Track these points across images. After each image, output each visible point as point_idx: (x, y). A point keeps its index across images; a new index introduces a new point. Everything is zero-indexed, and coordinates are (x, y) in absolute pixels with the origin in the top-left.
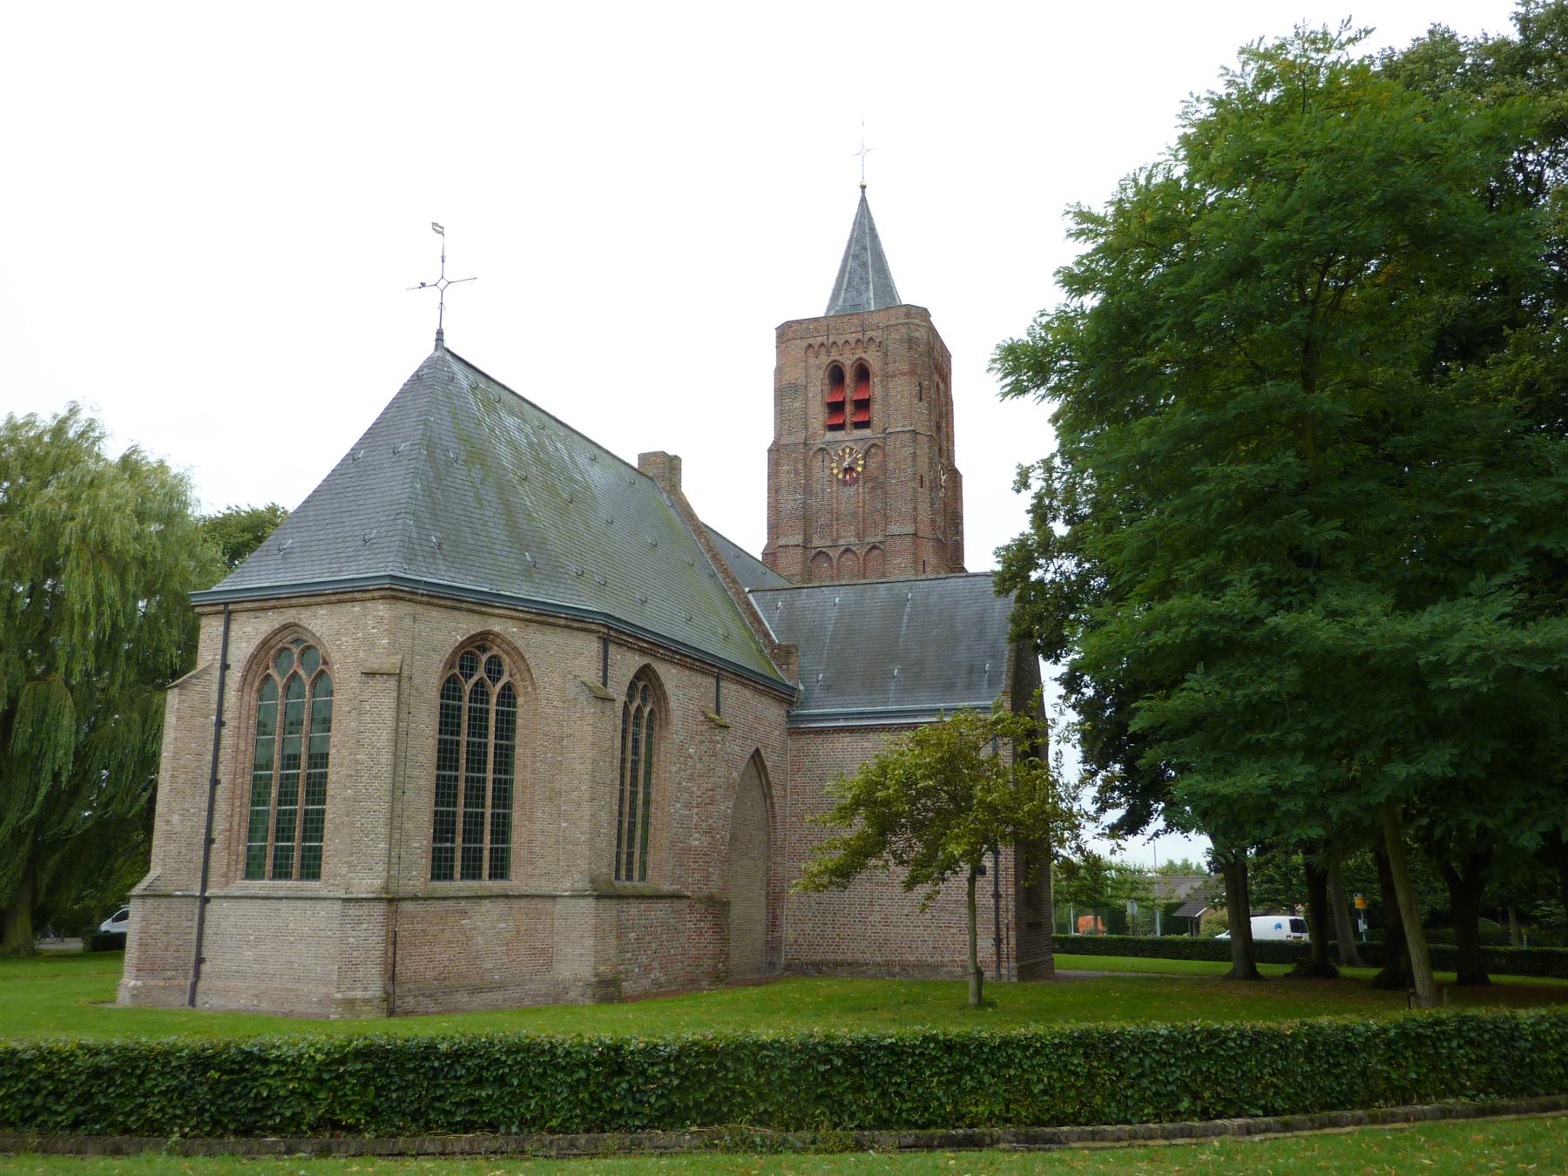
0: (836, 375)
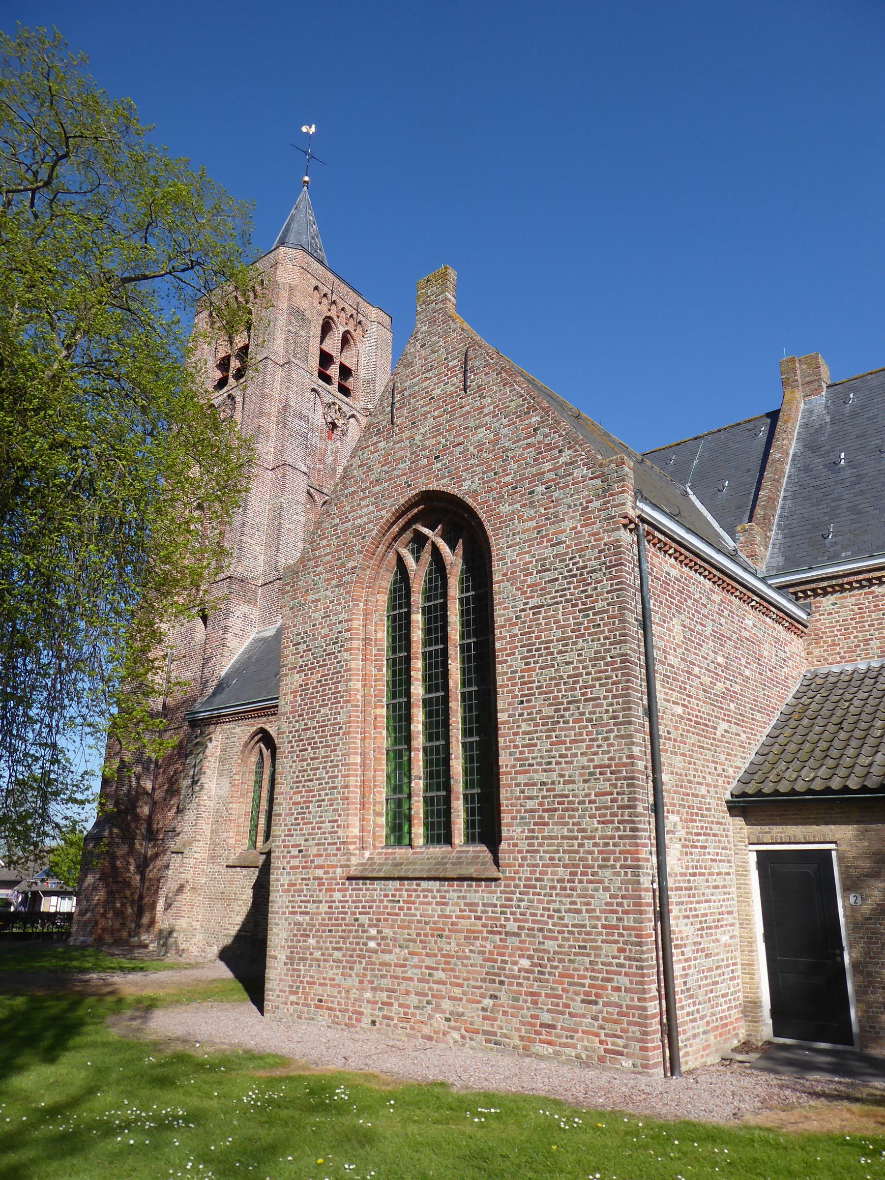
0: (327, 327)
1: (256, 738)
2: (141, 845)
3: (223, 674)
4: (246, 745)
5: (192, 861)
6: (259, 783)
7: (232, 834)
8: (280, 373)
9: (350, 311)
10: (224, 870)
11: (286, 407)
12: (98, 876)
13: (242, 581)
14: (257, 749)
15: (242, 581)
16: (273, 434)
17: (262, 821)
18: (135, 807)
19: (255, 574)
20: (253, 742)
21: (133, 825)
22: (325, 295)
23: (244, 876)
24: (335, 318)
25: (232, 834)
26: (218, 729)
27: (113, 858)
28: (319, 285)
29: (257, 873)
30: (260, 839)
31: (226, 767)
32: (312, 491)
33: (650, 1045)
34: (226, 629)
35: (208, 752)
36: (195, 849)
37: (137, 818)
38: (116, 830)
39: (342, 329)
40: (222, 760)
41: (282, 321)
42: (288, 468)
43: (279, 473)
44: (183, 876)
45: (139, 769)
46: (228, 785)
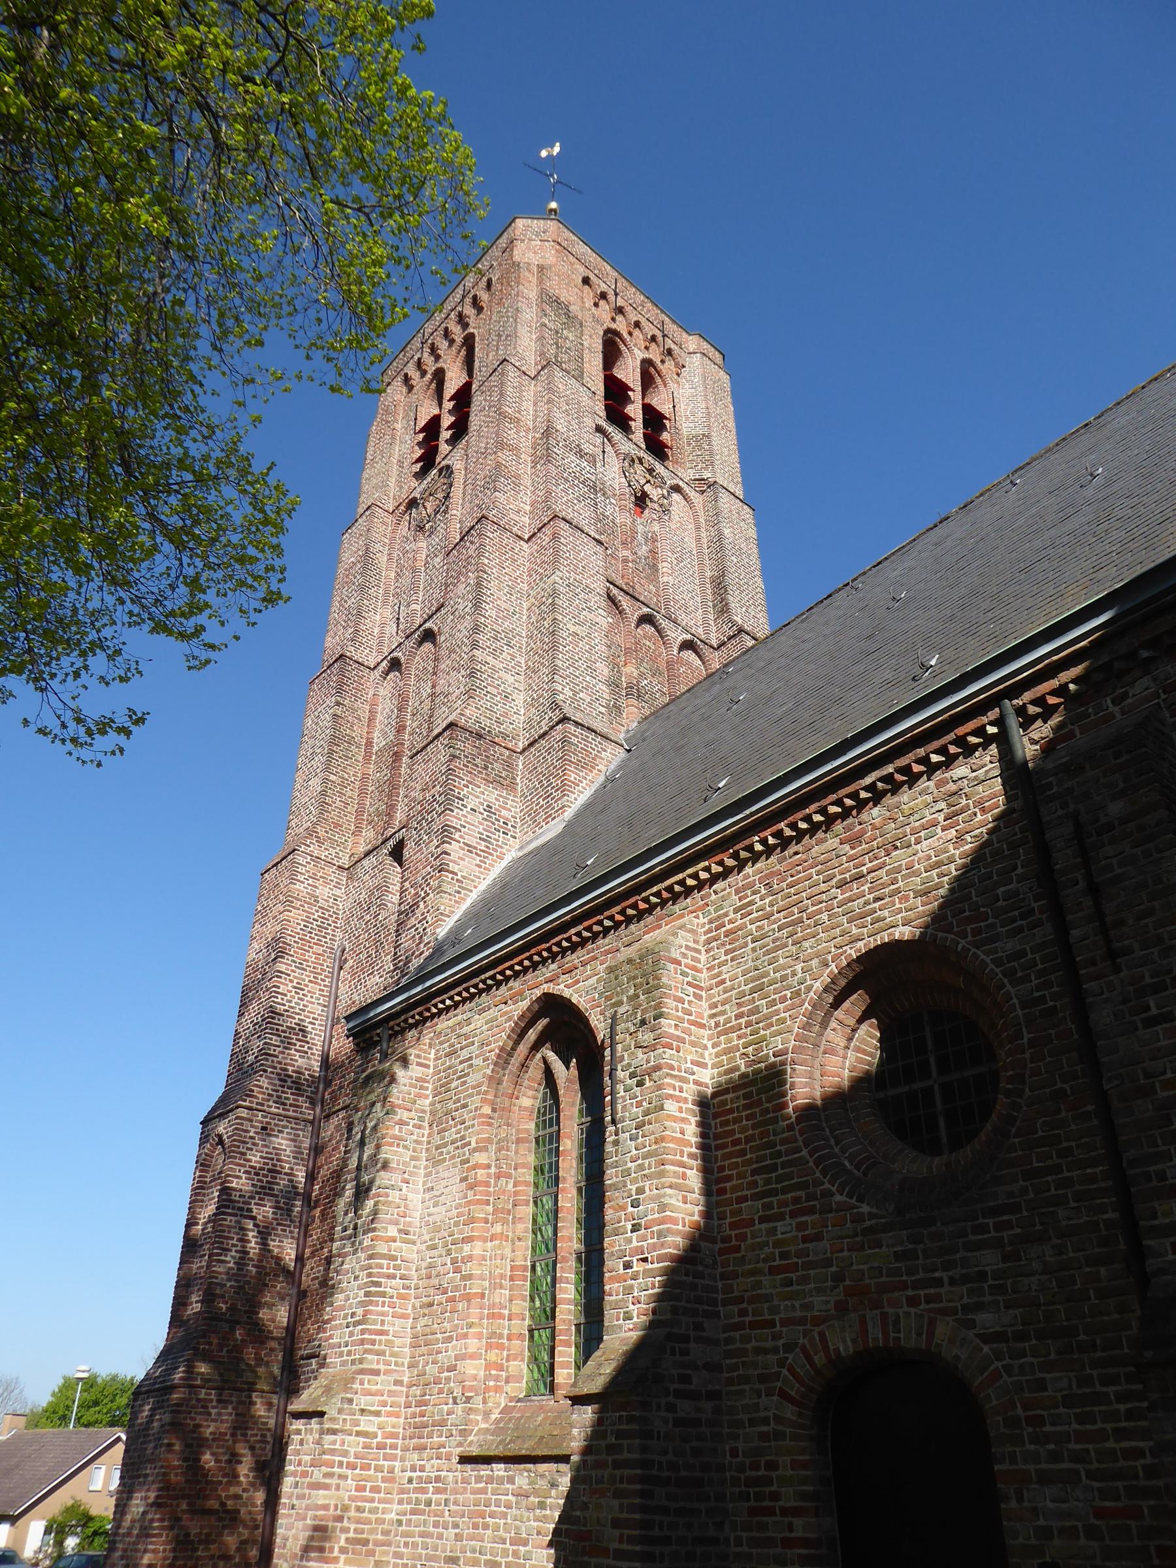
1: (532, 1035)
2: (270, 1405)
3: (442, 932)
4: (505, 1055)
5: (354, 1445)
6: (548, 1174)
7: (473, 1344)
8: (531, 390)
9: (651, 330)
10: (455, 1474)
11: (548, 432)
12: (152, 1495)
13: (480, 736)
14: (535, 1071)
15: (480, 736)
16: (527, 481)
17: (569, 1292)
18: (254, 1305)
19: (505, 728)
20: (523, 1049)
21: (250, 1353)
22: (603, 296)
23: (522, 1494)
24: (625, 335)
25: (473, 1344)
26: (428, 1035)
27: (194, 1445)
28: (592, 277)
29: (565, 1482)
30: (566, 1354)
31: (451, 1135)
32: (615, 591)
33: (637, 1501)
34: (446, 833)
35: (398, 1094)
36: (362, 1401)
37: (259, 1334)
38: (203, 1368)
39: (640, 355)
40: (439, 1119)
41: (529, 314)
42: (562, 524)
43: (545, 538)
44: (321, 1497)
45: (265, 1211)
46: (457, 1187)
